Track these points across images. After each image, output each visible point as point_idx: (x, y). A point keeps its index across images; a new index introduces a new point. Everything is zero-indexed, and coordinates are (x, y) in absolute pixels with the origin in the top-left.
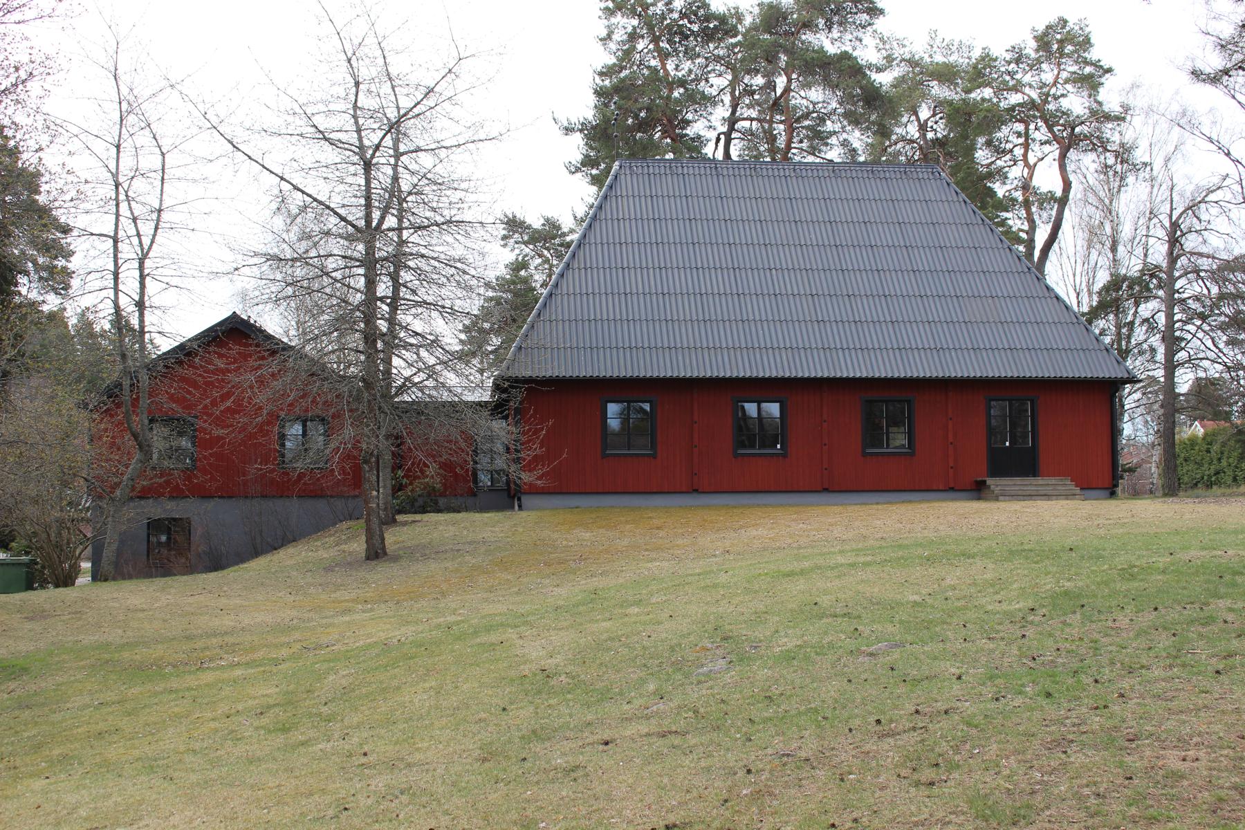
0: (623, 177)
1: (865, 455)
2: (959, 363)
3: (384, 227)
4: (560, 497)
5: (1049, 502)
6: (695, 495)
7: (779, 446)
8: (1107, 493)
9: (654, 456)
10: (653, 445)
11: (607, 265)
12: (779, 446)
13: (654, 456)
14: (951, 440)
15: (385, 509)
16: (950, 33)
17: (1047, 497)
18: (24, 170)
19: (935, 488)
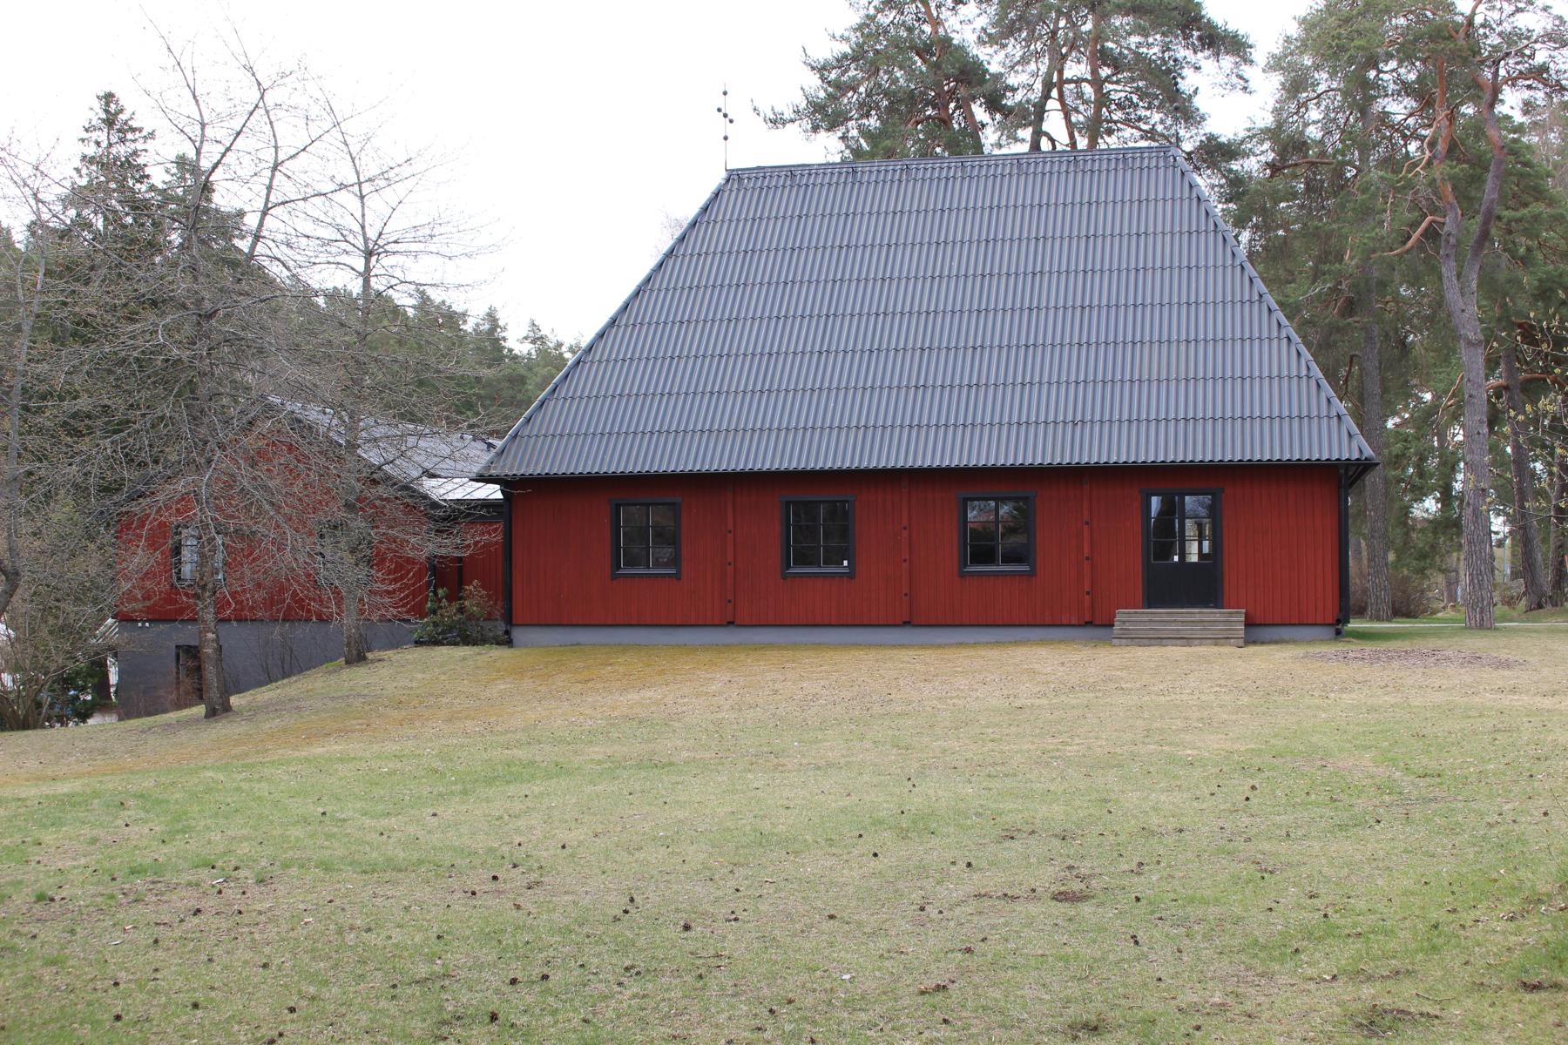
0: (727, 194)
1: (963, 575)
2: (546, 458)
3: (256, 253)
4: (560, 630)
5: (1164, 649)
6: (731, 629)
7: (845, 563)
8: (1330, 631)
9: (678, 577)
10: (675, 561)
11: (1247, 335)
12: (845, 563)
13: (678, 577)
14: (1086, 553)
15: (348, 644)
16: (1302, 12)
17: (1187, 641)
18: (217, 210)
19: (1064, 622)
